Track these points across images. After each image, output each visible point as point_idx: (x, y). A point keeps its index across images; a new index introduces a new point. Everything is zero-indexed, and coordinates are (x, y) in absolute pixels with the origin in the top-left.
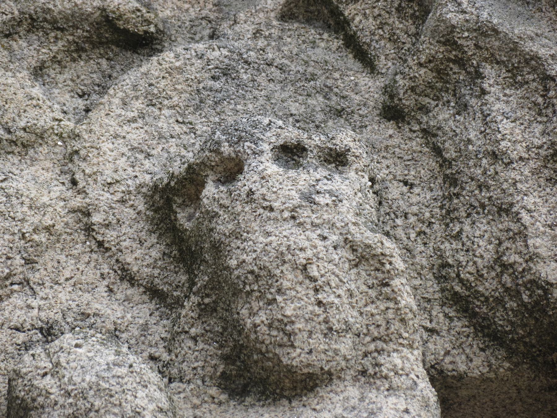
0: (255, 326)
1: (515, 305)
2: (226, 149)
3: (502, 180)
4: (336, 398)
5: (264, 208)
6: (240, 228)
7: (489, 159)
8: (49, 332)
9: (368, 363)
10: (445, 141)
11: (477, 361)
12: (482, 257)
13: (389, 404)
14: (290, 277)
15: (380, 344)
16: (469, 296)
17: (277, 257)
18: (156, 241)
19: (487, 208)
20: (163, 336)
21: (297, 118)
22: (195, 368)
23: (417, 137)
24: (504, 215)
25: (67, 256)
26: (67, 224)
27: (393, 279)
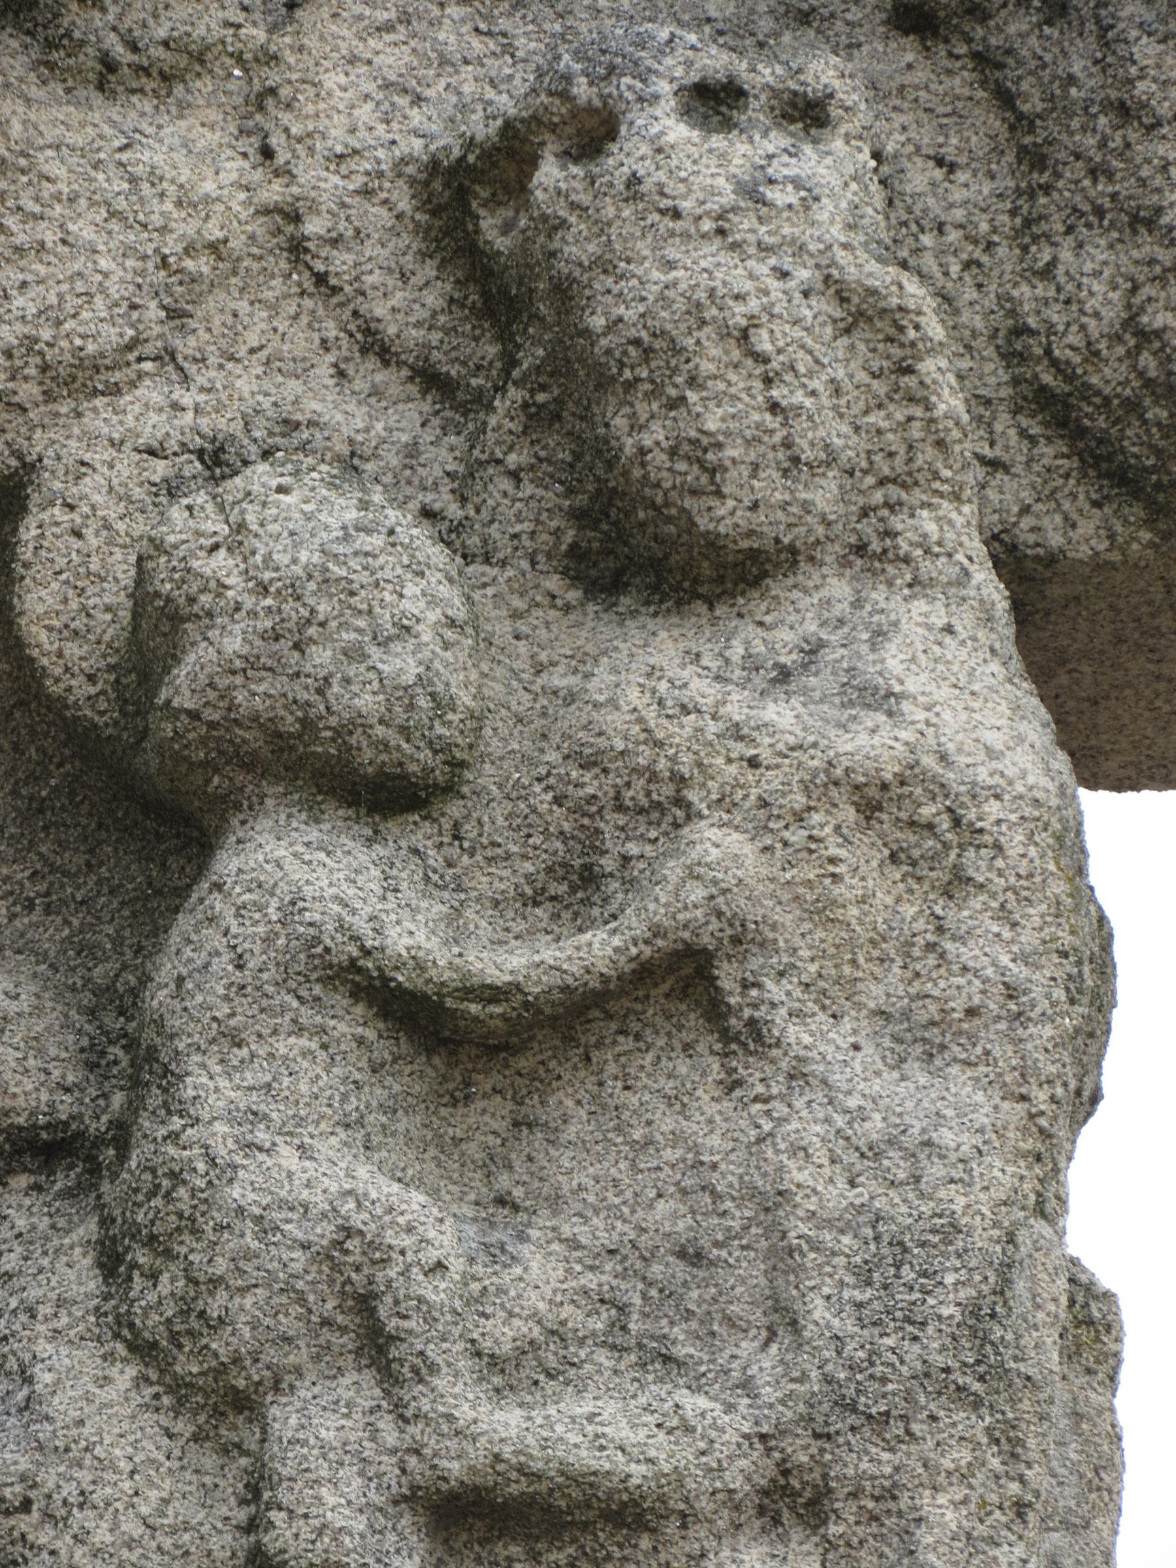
0: (642, 451)
1: (1165, 414)
2: (582, 90)
3: (1138, 160)
4: (805, 602)
5: (662, 212)
6: (613, 251)
7: (1112, 116)
8: (217, 460)
9: (869, 530)
10: (1020, 78)
11: (1086, 528)
12: (1097, 315)
13: (914, 614)
14: (714, 352)
15: (894, 492)
16: (1070, 394)
17: (688, 312)
18: (434, 273)
19: (1109, 216)
20: (449, 468)
21: (720, 25)
22: (515, 536)
23: (963, 68)
24: (1143, 230)
25: (252, 303)
26: (252, 237)
27: (922, 360)
